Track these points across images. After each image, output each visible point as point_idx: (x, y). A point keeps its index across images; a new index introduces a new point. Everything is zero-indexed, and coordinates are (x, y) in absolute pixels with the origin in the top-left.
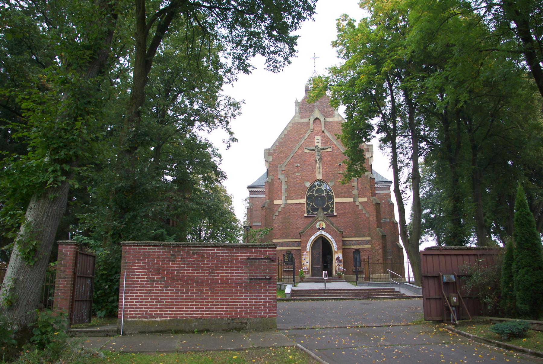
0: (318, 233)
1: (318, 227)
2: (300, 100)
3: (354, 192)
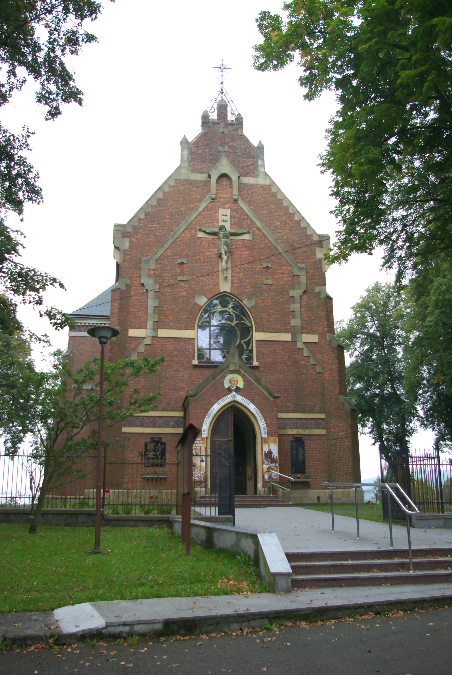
0: (228, 399)
1: (227, 385)
2: (191, 138)
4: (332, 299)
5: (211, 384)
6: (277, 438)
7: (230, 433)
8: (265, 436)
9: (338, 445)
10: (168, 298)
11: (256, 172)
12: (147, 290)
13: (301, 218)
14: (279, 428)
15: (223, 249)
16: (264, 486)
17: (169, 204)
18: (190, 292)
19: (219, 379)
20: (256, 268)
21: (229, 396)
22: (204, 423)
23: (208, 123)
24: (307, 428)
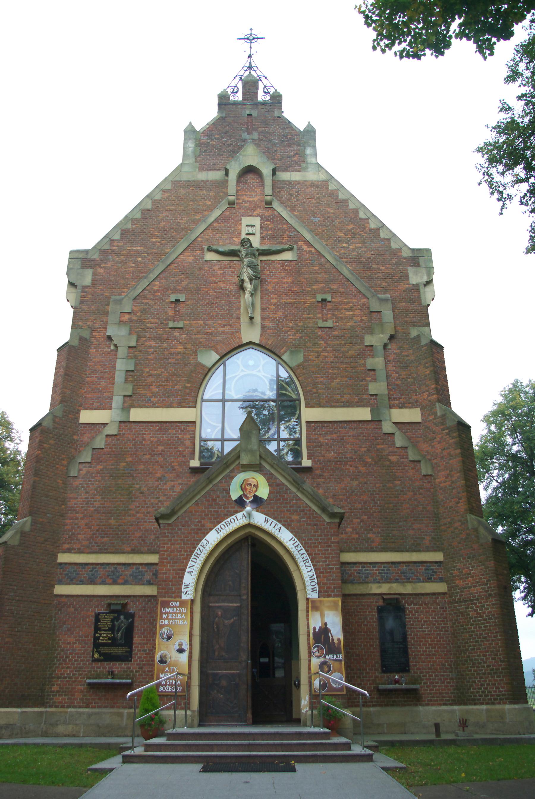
0: (237, 521)
1: (235, 494)
2: (199, 126)
3: (373, 388)
4: (442, 348)
5: (203, 493)
6: (339, 600)
7: (244, 591)
8: (315, 595)
9: (472, 614)
10: (151, 357)
11: (303, 165)
12: (115, 346)
13: (380, 225)
14: (344, 581)
15: (246, 274)
16: (312, 706)
17: (161, 216)
18: (189, 346)
19: (220, 482)
20: (305, 303)
21: (239, 515)
22: (188, 570)
23: (227, 104)
24: (409, 580)
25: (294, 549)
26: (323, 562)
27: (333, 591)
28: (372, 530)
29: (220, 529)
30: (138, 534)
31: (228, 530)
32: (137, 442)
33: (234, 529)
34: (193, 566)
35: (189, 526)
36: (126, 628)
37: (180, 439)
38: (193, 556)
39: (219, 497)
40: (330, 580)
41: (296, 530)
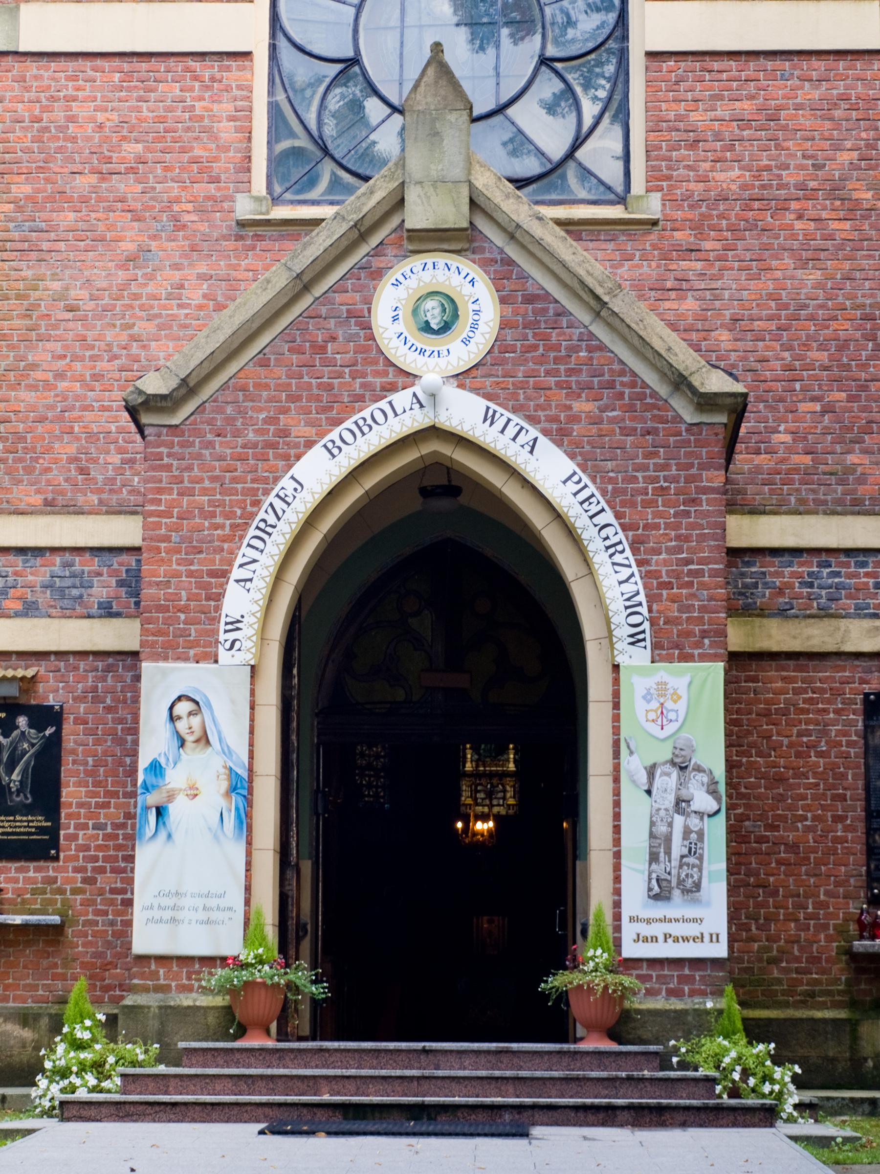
22: (237, 573)
25: (578, 509)
26: (669, 551)
27: (699, 645)
28: (861, 441)
29: (339, 443)
30: (66, 449)
31: (365, 448)
32: (47, 129)
33: (384, 443)
34: (255, 561)
35: (237, 434)
36: (38, 756)
37: (202, 118)
38: (252, 532)
39: (333, 339)
40: (689, 608)
41: (587, 448)
